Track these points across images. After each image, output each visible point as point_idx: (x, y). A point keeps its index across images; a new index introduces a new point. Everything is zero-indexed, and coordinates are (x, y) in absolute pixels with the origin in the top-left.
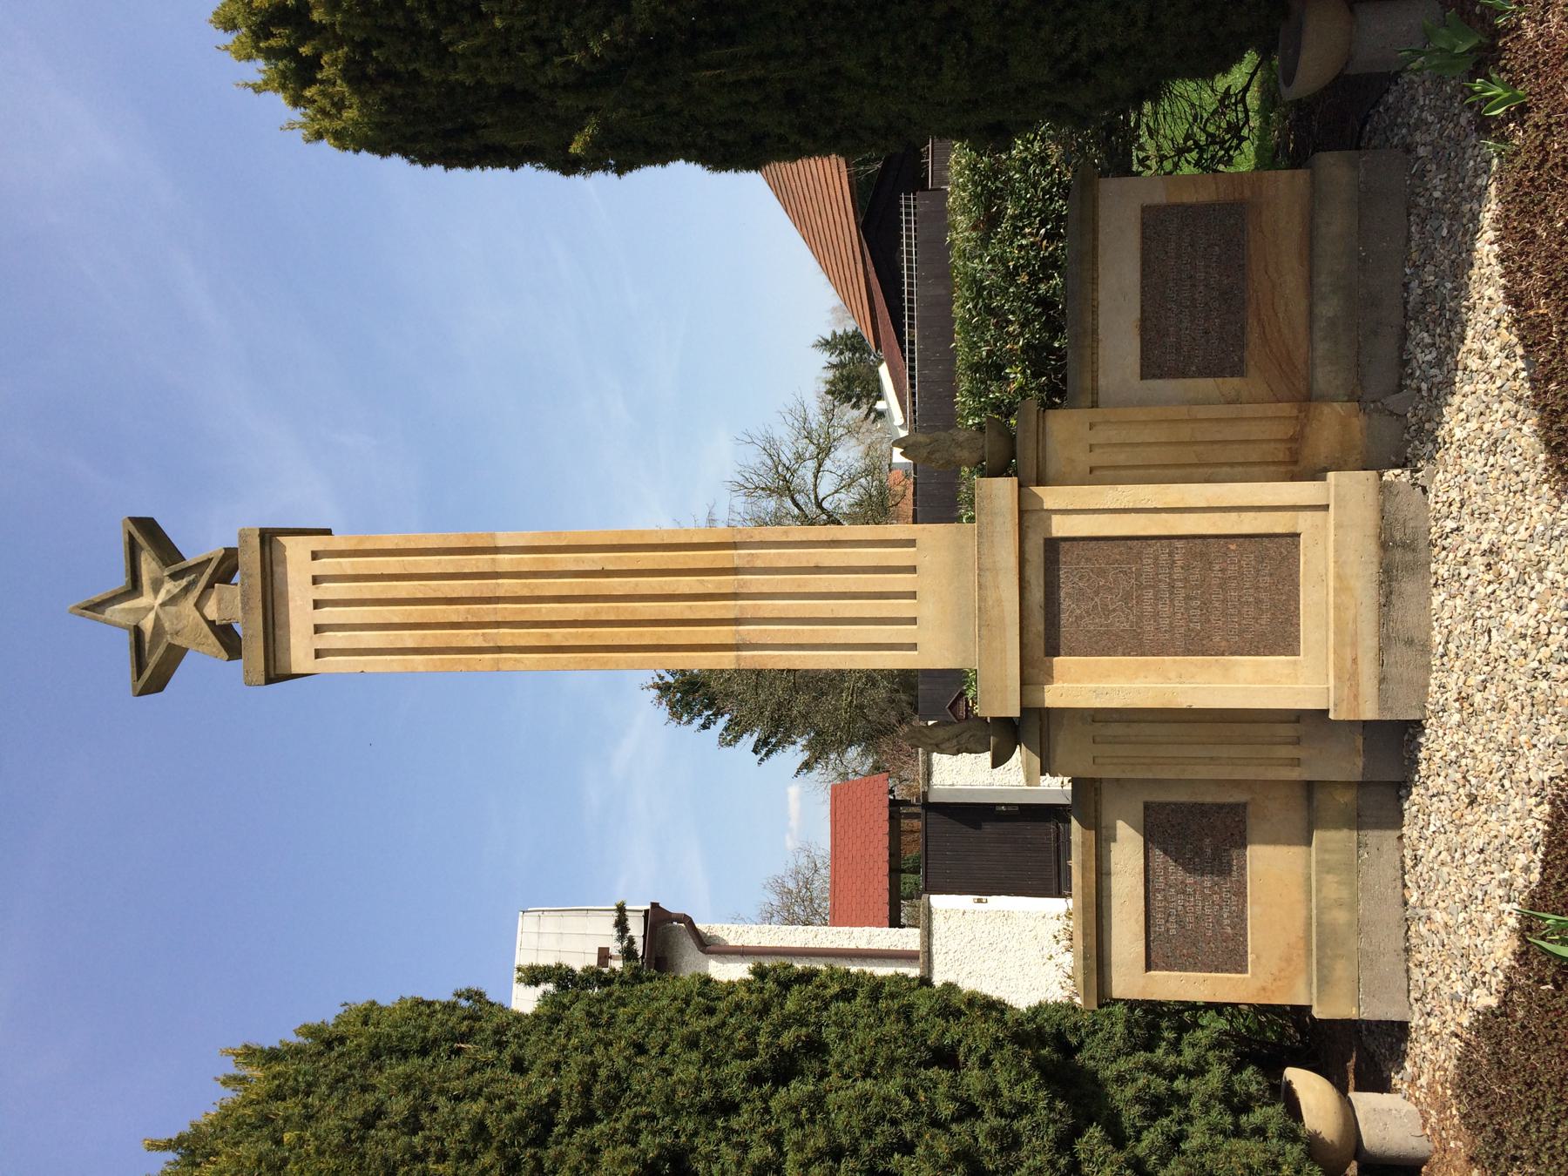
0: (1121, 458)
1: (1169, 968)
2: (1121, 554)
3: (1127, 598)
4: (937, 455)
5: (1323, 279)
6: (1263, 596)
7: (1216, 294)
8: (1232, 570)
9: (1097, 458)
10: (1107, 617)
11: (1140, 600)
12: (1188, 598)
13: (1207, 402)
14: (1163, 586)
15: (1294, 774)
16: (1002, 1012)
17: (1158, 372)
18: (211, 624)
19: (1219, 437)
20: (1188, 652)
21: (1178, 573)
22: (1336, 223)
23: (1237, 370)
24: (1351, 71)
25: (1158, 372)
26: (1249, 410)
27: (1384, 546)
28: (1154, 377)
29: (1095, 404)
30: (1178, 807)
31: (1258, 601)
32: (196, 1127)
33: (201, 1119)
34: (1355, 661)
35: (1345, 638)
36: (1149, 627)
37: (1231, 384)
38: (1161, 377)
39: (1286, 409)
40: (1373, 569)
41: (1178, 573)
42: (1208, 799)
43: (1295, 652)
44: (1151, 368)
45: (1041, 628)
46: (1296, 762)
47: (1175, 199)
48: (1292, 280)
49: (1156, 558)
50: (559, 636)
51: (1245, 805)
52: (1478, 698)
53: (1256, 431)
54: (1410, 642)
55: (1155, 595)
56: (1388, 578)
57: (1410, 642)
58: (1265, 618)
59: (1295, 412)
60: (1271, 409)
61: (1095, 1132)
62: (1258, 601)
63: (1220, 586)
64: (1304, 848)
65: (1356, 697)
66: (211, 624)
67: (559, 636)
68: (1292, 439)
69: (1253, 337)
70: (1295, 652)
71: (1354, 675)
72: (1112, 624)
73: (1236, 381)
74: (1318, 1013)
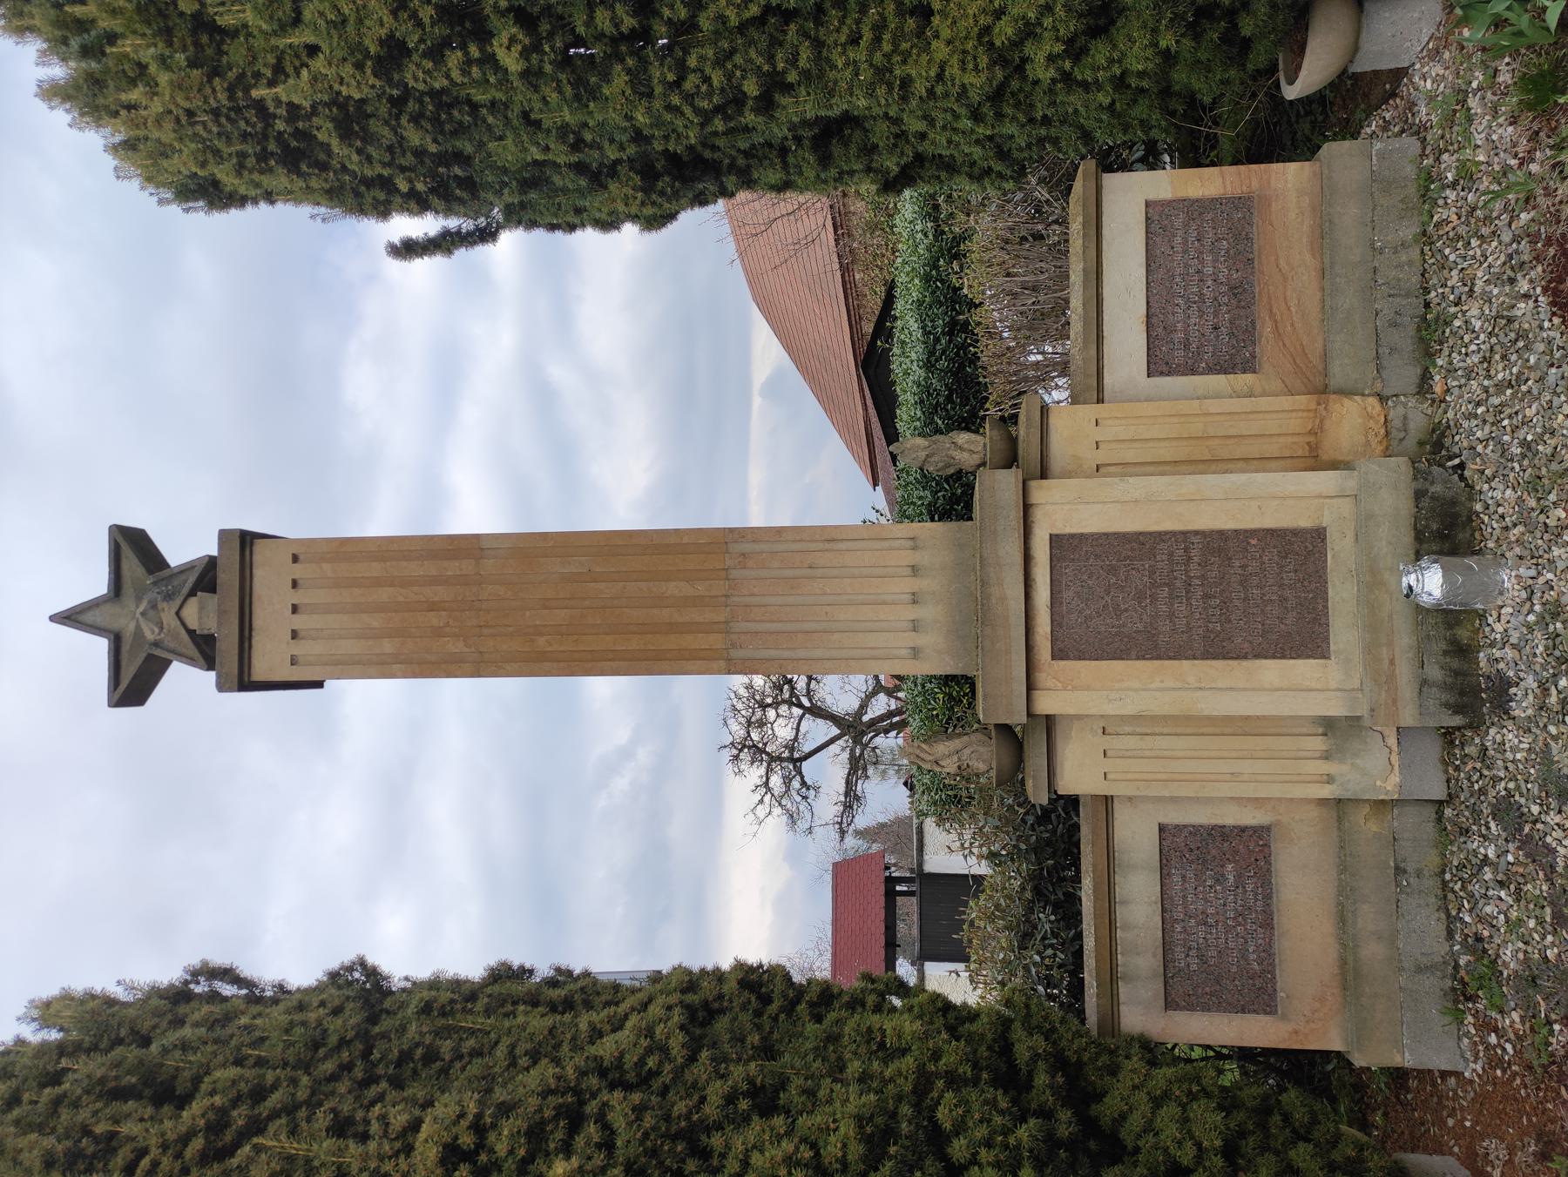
0: (1130, 455)
1: (1191, 1007)
2: (1132, 550)
3: (1140, 597)
4: (936, 458)
6: (1287, 593)
7: (1224, 289)
8: (1253, 566)
9: (1101, 456)
10: (1118, 617)
11: (1154, 598)
12: (1206, 596)
13: (1218, 396)
14: (1178, 583)
15: (1326, 792)
17: (1165, 369)
18: (191, 633)
19: (1233, 432)
20: (1207, 655)
21: (1195, 570)
23: (1249, 366)
24: (1357, 68)
25: (1165, 369)
26: (1263, 403)
28: (1162, 374)
29: (1100, 400)
30: (1195, 830)
31: (1283, 599)
32: (761, 966)
33: (765, 962)
34: (1392, 662)
36: (1165, 627)
37: (1244, 380)
38: (1169, 374)
39: (1303, 401)
41: (1195, 570)
42: (1229, 820)
44: (1157, 365)
45: (1048, 629)
46: (1330, 779)
47: (1181, 194)
49: (1171, 554)
51: (1268, 829)
55: (1171, 594)
58: (1291, 618)
59: (1313, 406)
60: (1286, 402)
62: (1283, 599)
63: (1241, 583)
65: (1395, 701)
66: (191, 633)
68: (1311, 432)
69: (1266, 330)
71: (1391, 678)
72: (1124, 625)
73: (1249, 377)
74: (1359, 1061)
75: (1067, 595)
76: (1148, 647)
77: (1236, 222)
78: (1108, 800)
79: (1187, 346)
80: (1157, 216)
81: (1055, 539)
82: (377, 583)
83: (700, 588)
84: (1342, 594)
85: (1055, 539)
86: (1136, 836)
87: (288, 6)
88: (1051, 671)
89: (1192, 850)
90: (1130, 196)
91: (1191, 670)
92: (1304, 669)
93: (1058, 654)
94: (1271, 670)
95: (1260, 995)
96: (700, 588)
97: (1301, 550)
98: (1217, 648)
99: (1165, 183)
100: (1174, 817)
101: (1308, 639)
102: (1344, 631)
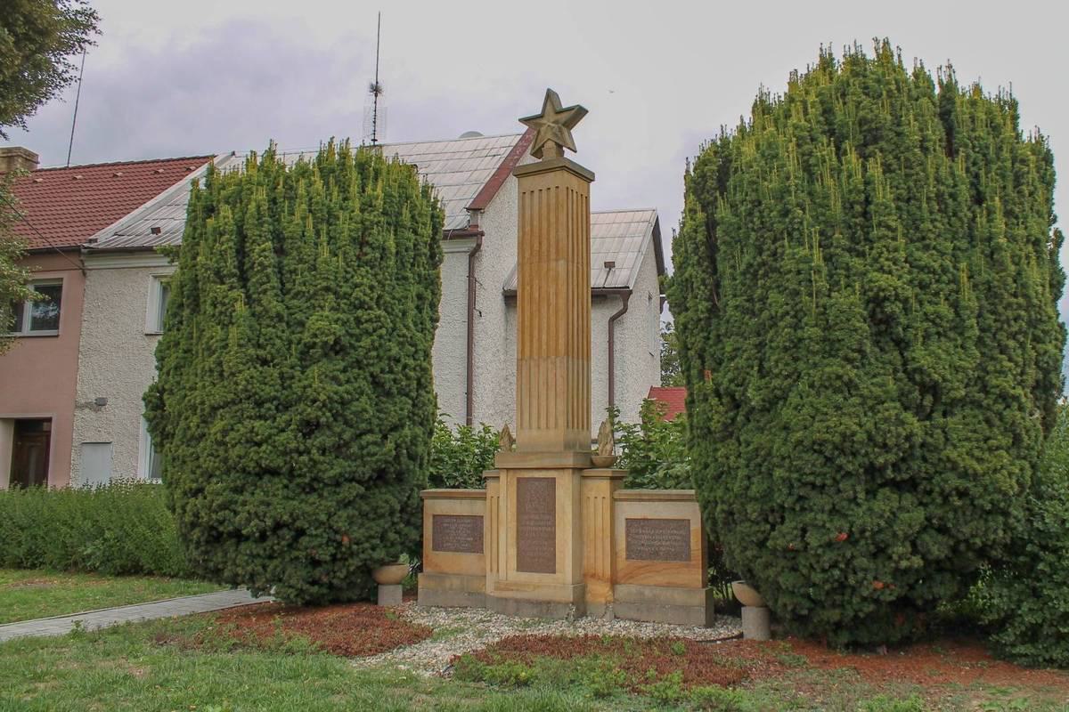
5: (657, 591)
16: (161, 351)
22: (679, 597)
27: (549, 603)
28: (627, 524)
35: (518, 586)
40: (541, 598)
43: (518, 570)
48: (660, 579)
50: (570, 327)
52: (855, 600)
53: (599, 563)
54: (518, 610)
56: (537, 604)
57: (518, 610)
61: (362, 490)
64: (743, 609)
67: (570, 327)
70: (518, 570)
71: (508, 590)
75: (537, 483)
76: (521, 511)
77: (682, 555)
78: (485, 499)
79: (637, 534)
80: (684, 524)
81: (554, 479)
82: (532, 225)
83: (544, 347)
84: (535, 577)
85: (554, 479)
86: (476, 508)
87: (8, 659)
88: (513, 477)
89: (475, 524)
90: (691, 513)
91: (513, 525)
92: (513, 563)
93: (519, 480)
94: (513, 552)
95: (437, 547)
96: (544, 347)
97: (549, 565)
98: (520, 535)
99: (696, 526)
100: (486, 523)
101: (522, 566)
102: (525, 577)
